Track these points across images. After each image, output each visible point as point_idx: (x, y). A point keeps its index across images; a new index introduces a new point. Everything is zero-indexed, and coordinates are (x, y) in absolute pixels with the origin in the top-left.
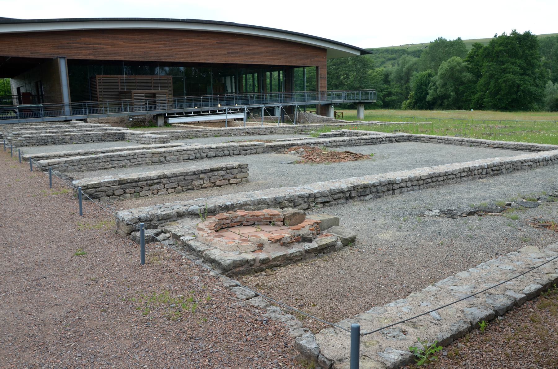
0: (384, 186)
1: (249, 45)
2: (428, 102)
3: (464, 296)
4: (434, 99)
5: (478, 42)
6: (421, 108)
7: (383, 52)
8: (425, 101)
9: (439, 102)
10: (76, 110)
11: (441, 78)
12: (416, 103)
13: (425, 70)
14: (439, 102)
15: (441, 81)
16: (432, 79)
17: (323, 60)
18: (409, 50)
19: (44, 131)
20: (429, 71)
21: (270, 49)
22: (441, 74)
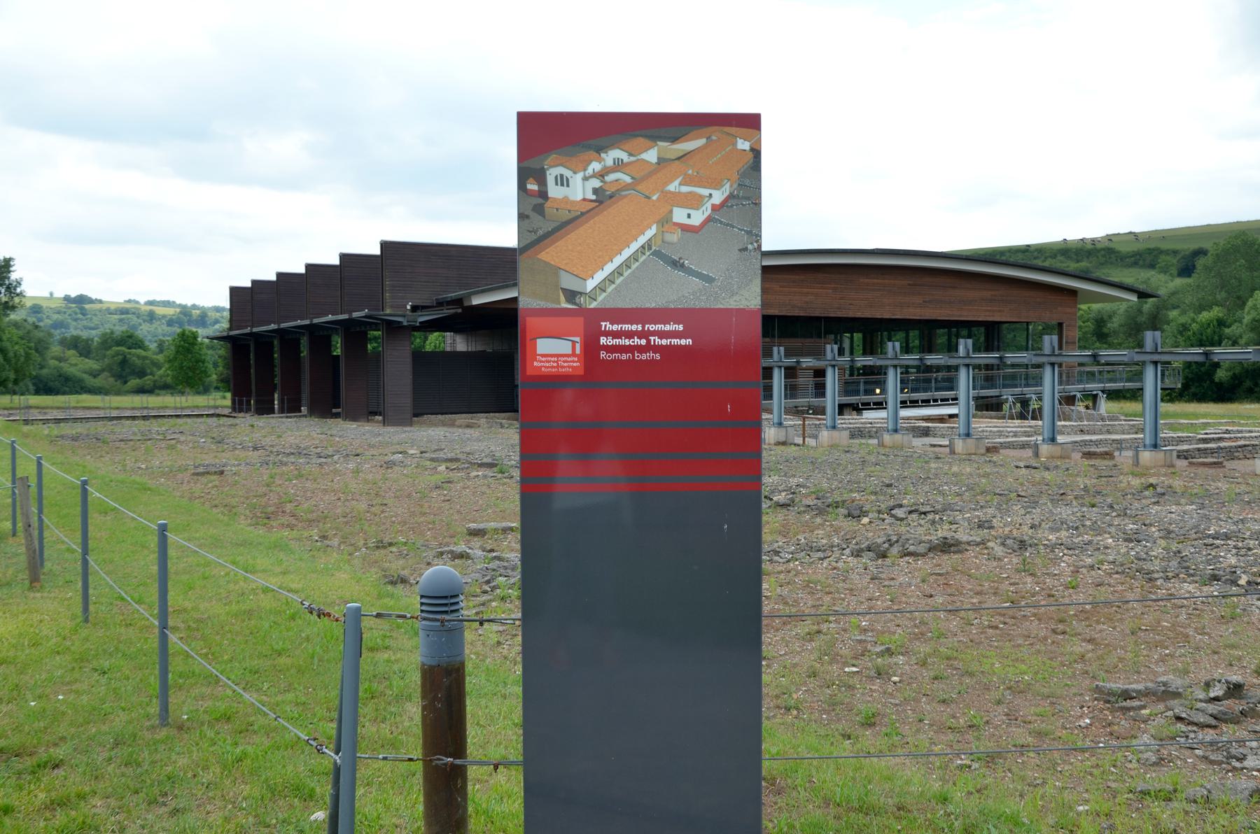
0: (837, 505)
1: (955, 288)
2: (1220, 384)
3: (123, 421)
4: (1234, 377)
5: (1244, 233)
6: (1201, 398)
7: (1054, 256)
8: (1212, 381)
9: (1248, 383)
10: (282, 411)
11: (1252, 330)
12: (1186, 386)
13: (1201, 308)
14: (1248, 383)
15: (1252, 335)
16: (1227, 331)
17: (1069, 310)
18: (1124, 249)
19: (35, 414)
20: (1216, 312)
21: (987, 294)
22: (1254, 320)
